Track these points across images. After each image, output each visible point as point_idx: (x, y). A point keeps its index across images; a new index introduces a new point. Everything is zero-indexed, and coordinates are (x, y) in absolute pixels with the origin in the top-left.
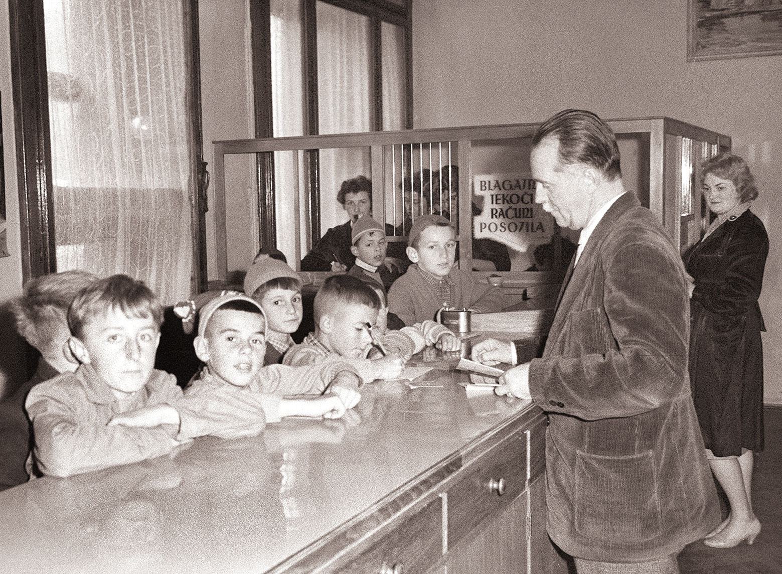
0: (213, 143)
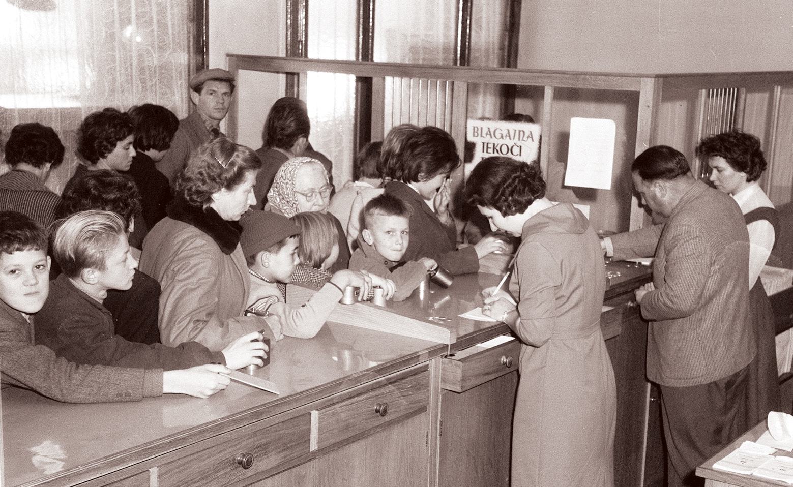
0: (228, 55)
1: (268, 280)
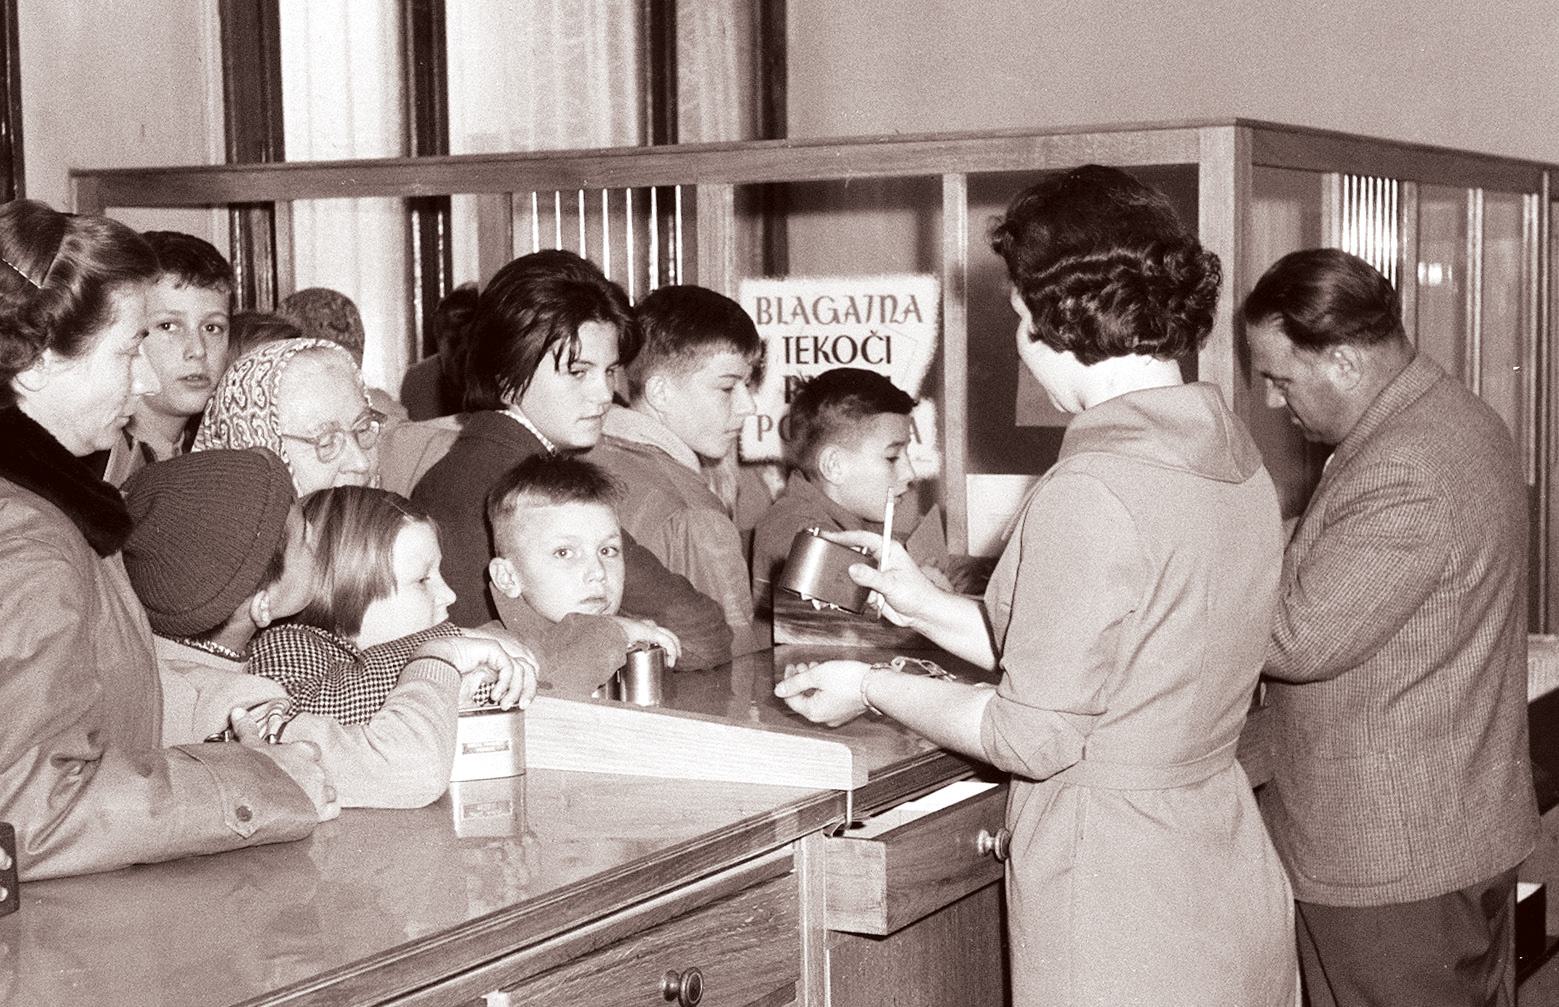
1: (233, 654)
